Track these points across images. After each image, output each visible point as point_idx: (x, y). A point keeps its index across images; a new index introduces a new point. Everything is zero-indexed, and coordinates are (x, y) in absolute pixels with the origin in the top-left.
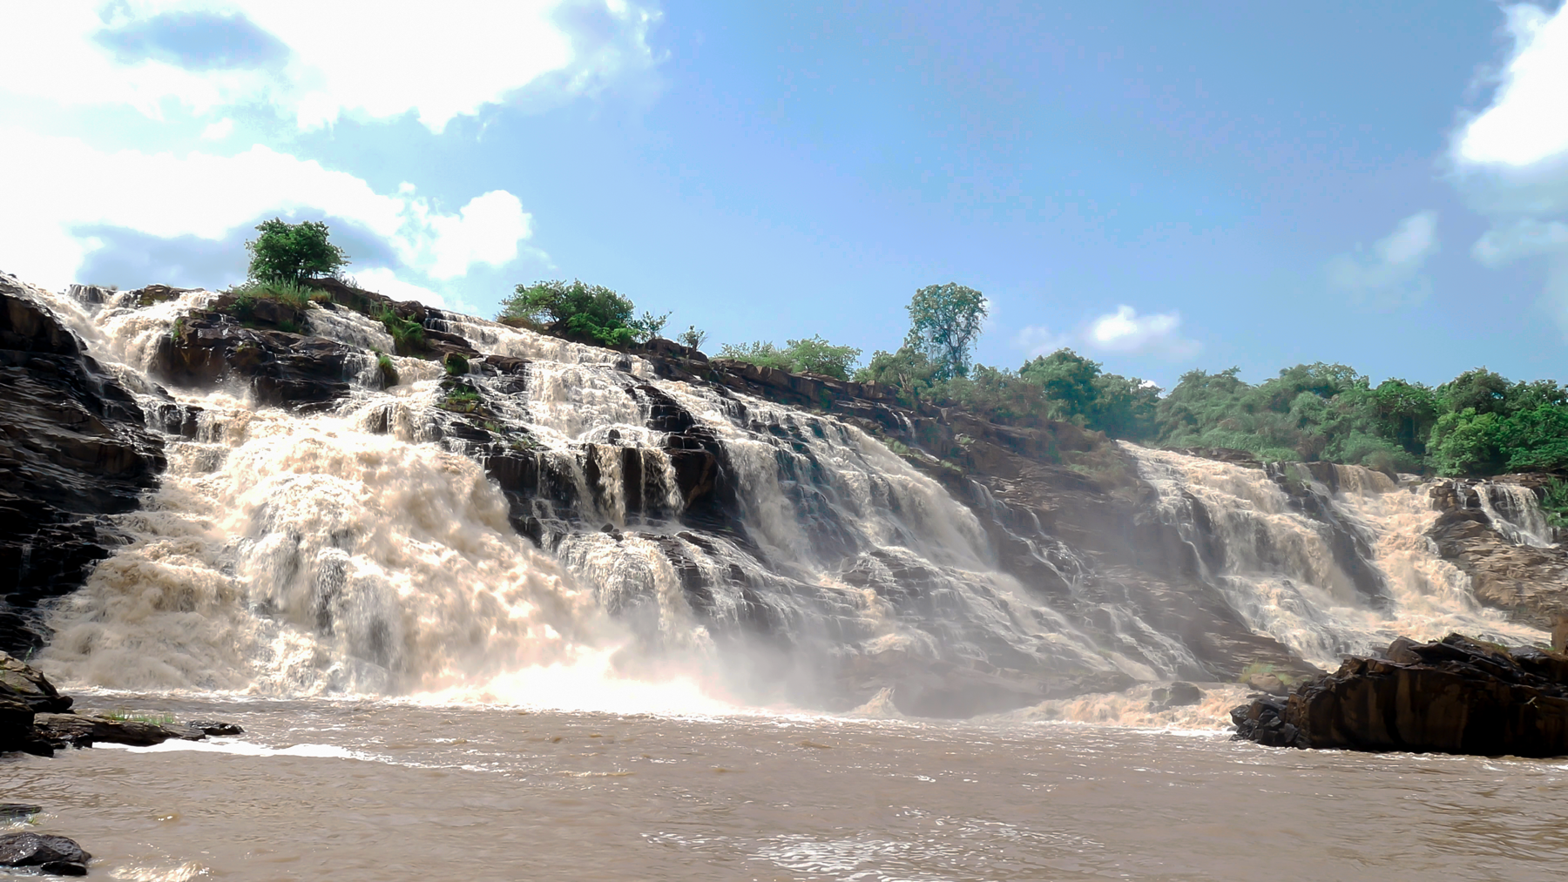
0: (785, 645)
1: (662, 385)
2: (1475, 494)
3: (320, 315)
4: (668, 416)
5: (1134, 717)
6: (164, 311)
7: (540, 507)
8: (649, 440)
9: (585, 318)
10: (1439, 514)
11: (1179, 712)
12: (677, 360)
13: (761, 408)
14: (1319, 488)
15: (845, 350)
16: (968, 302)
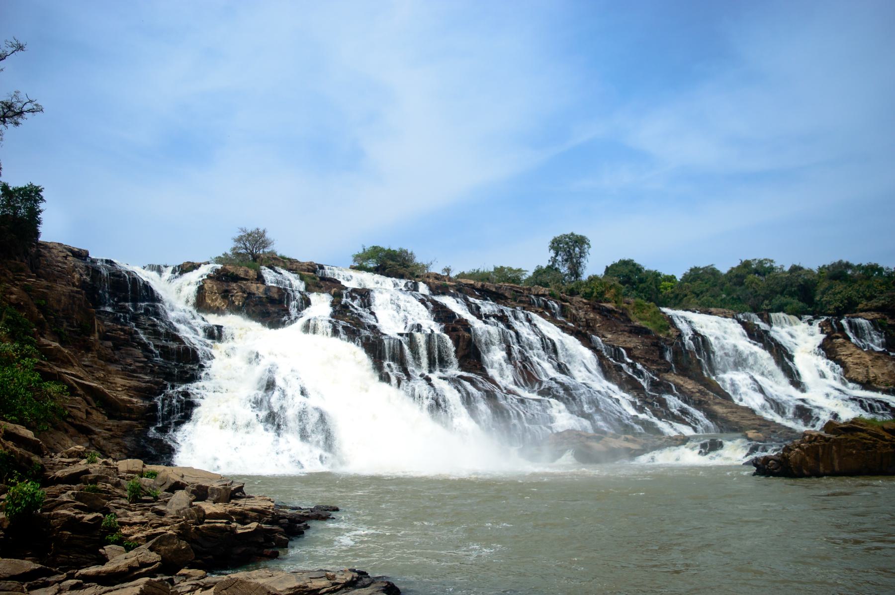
0: (509, 429)
1: (436, 298)
2: (842, 325)
3: (269, 275)
4: (442, 314)
5: (690, 457)
6: (194, 277)
7: (389, 366)
8: (430, 324)
9: (391, 263)
10: (824, 336)
11: (712, 454)
12: (440, 286)
13: (488, 307)
14: (764, 326)
15: (520, 270)
16: (580, 241)
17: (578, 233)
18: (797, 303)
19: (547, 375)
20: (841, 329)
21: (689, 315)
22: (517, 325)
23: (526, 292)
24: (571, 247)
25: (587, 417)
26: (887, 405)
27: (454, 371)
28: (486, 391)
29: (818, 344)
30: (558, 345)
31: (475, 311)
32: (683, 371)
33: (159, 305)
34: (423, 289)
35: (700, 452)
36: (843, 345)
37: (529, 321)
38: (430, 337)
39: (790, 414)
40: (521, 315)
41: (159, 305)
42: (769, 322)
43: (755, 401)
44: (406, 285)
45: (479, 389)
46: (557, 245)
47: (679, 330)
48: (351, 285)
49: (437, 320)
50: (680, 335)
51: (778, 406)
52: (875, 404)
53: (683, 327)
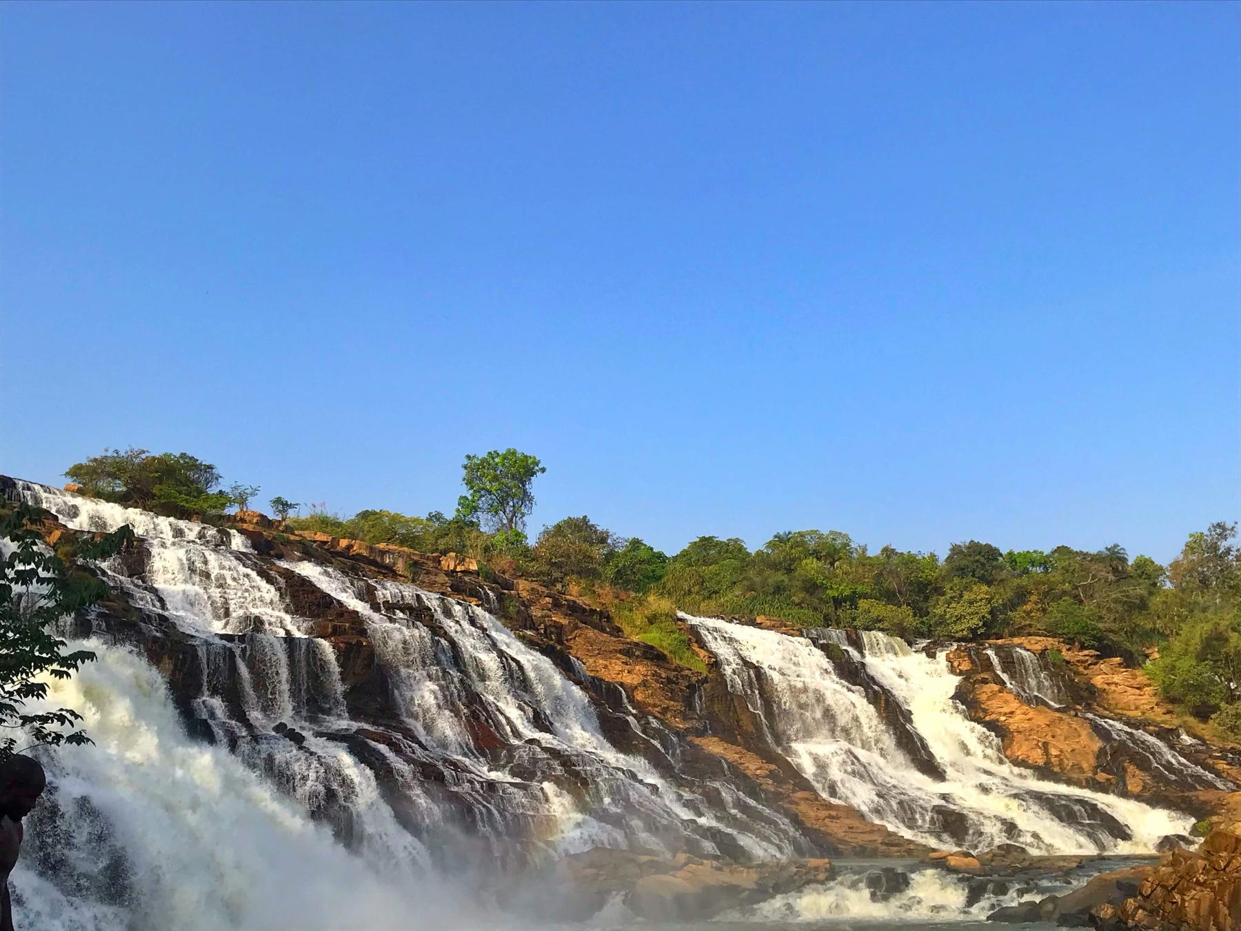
4: (301, 597)
8: (283, 623)
17: (523, 449)
18: (905, 614)
20: (988, 666)
21: (735, 630)
22: (449, 625)
23: (431, 564)
24: (506, 479)
25: (617, 821)
26: (1094, 807)
28: (423, 765)
29: (952, 692)
30: (532, 675)
31: (367, 595)
32: (728, 734)
34: (238, 542)
35: (873, 895)
36: (993, 695)
39: (924, 820)
40: (457, 609)
42: (859, 647)
43: (861, 796)
44: (201, 536)
45: (409, 761)
46: (476, 471)
47: (713, 655)
49: (296, 609)
50: (716, 664)
51: (907, 811)
52: (1077, 808)
53: (722, 650)
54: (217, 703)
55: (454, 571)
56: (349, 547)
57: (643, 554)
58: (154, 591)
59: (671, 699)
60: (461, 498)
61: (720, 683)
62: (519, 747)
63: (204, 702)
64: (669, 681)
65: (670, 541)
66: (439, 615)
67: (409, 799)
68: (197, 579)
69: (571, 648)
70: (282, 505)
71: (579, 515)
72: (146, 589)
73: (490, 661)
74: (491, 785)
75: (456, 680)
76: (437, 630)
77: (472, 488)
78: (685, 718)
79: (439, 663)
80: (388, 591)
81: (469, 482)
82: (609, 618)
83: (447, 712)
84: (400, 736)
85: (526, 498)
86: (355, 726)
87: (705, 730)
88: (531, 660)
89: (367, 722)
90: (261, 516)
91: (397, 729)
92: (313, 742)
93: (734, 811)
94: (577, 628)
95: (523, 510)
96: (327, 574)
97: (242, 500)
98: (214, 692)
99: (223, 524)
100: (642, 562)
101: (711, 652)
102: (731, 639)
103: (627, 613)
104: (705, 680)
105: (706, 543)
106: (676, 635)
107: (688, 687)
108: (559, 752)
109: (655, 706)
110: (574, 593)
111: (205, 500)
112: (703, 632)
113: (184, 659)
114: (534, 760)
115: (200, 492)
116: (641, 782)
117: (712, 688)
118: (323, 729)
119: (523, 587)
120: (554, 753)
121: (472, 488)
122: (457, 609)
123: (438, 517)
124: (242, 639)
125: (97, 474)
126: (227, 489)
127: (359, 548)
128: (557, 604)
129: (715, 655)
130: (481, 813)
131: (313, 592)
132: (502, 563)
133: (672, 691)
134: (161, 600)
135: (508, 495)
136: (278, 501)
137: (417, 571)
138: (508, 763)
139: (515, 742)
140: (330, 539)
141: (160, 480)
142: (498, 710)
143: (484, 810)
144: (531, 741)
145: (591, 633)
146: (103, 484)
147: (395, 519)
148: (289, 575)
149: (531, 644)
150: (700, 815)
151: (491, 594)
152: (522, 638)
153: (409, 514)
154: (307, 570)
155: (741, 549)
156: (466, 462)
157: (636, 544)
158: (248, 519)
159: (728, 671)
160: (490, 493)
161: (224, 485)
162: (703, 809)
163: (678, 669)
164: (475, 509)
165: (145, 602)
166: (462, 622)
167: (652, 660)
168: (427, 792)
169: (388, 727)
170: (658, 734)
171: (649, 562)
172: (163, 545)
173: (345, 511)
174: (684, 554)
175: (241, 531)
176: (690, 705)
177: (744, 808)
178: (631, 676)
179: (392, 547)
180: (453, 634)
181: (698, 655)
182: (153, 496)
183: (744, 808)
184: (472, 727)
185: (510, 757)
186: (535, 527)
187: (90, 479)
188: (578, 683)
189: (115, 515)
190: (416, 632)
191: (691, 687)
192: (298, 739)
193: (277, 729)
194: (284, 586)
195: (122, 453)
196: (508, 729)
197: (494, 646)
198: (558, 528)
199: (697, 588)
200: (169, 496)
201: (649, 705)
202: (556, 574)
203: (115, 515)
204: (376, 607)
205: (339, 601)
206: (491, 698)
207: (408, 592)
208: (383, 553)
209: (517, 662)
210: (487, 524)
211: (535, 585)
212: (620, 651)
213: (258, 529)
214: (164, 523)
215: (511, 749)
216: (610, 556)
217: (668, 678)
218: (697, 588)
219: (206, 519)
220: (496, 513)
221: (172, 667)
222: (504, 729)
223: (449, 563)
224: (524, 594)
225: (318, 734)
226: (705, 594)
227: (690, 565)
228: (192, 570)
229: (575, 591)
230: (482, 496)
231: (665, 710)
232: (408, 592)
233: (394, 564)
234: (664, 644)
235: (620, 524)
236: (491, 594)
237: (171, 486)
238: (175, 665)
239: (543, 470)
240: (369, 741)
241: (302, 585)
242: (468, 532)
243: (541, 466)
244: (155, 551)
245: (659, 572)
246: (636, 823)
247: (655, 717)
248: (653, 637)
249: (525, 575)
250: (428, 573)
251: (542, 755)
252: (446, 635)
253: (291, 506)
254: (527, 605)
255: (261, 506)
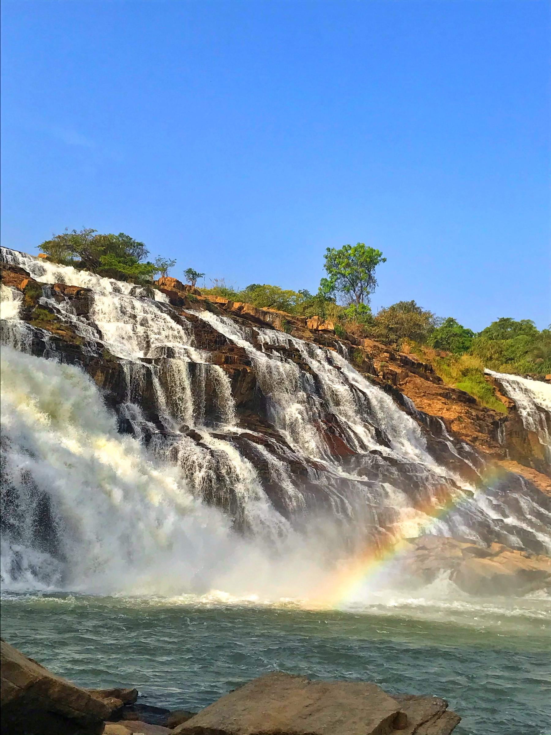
4: (204, 337)
8: (187, 353)
17: (369, 244)
19: (363, 446)
22: (314, 365)
23: (300, 324)
24: (357, 267)
27: (231, 427)
31: (253, 338)
33: (391, 535)
37: (330, 361)
38: (192, 367)
40: (319, 352)
41: (391, 535)
44: (132, 293)
45: (281, 458)
46: (334, 261)
48: (48, 278)
49: (199, 345)
50: (514, 408)
53: (518, 396)
54: (136, 408)
55: (317, 330)
56: (241, 308)
57: (455, 330)
58: (96, 327)
59: (479, 431)
60: (323, 279)
61: (518, 422)
62: (364, 456)
63: (127, 407)
64: (478, 418)
65: (477, 322)
66: (305, 355)
67: (281, 489)
68: (126, 318)
69: (403, 390)
70: (193, 275)
71: (407, 299)
72: (89, 324)
73: (342, 390)
74: (344, 481)
75: (317, 403)
76: (303, 366)
77: (331, 272)
78: (490, 447)
79: (305, 390)
80: (266, 336)
81: (329, 269)
82: (432, 371)
83: (309, 426)
84: (274, 440)
85: (370, 280)
86: (240, 431)
87: (505, 456)
88: (375, 393)
89: (250, 429)
90: (177, 281)
91: (271, 435)
92: (207, 438)
93: (529, 517)
94: (407, 376)
95: (368, 289)
96: (222, 322)
97: (164, 270)
98: (134, 400)
99: (147, 287)
100: (455, 335)
101: (511, 399)
102: (526, 390)
103: (445, 367)
104: (506, 420)
105: (504, 323)
106: (484, 385)
107: (492, 424)
108: (396, 461)
109: (467, 436)
110: (406, 351)
111: (136, 268)
112: (504, 384)
113: (113, 372)
114: (376, 466)
115: (133, 262)
116: (459, 488)
117: (512, 425)
118: (217, 432)
119: (368, 344)
120: (392, 462)
121: (331, 272)
122: (319, 352)
123: (305, 294)
124: (157, 361)
125: (60, 247)
126: (153, 261)
127: (248, 309)
128: (392, 358)
129: (514, 402)
130: (336, 502)
131: (212, 332)
132: (353, 327)
133: (480, 426)
134: (99, 332)
135: (357, 278)
136: (190, 271)
137: (289, 326)
138: (356, 467)
139: (363, 452)
140: (227, 302)
141: (105, 253)
142: (350, 428)
143: (338, 499)
144: (375, 452)
145: (419, 380)
146: (67, 255)
147: (274, 291)
148: (194, 319)
149: (374, 382)
150: (506, 516)
151: (344, 347)
152: (368, 378)
153: (284, 288)
154: (207, 316)
155: (531, 328)
156: (326, 253)
157: (451, 322)
158: (168, 283)
159: (524, 413)
160: (344, 276)
161: (151, 258)
162: (507, 512)
163: (485, 410)
164: (333, 288)
165: (86, 333)
166: (322, 362)
167: (465, 402)
168: (294, 483)
169: (265, 433)
170: (468, 455)
171: (460, 336)
172: (103, 294)
173: (239, 286)
174: (487, 331)
175: (163, 291)
176: (494, 437)
177: (539, 515)
178: (448, 413)
179: (271, 310)
180: (315, 370)
181: (500, 400)
182: (100, 263)
183: (539, 515)
184: (329, 439)
185: (358, 463)
186: (379, 302)
187: (55, 251)
188: (409, 413)
189: (78, 278)
190: (287, 365)
191: (496, 424)
192: (196, 437)
193: (181, 430)
194: (190, 327)
195: (78, 233)
196: (356, 443)
197: (346, 380)
198: (393, 309)
199: (497, 355)
200: (111, 264)
201: (463, 434)
202: (393, 337)
203: (78, 278)
204: (258, 347)
205: (231, 341)
206: (343, 419)
207: (283, 337)
208: (265, 313)
209: (364, 393)
210: (341, 299)
211: (376, 344)
212: (440, 395)
213: (174, 290)
214: (106, 283)
215: (359, 457)
216: (432, 330)
217: (477, 416)
218: (497, 355)
219: (135, 280)
220: (348, 291)
221: (103, 378)
222: (353, 442)
223: (313, 324)
224: (368, 349)
225: (216, 436)
226: (506, 360)
227: (491, 339)
228: (124, 313)
229: (406, 349)
230: (338, 279)
231: (475, 439)
232: (283, 337)
233: (273, 322)
234: (474, 391)
235: (439, 308)
236: (344, 347)
237: (112, 257)
238: (106, 378)
239: (384, 260)
240: (250, 442)
241: (204, 327)
242: (328, 305)
243: (382, 257)
244: (96, 297)
245: (467, 344)
246: (457, 518)
247: (467, 444)
248: (466, 386)
249: (368, 336)
250: (298, 329)
251: (382, 462)
252: (310, 370)
253: (199, 276)
254: (371, 357)
255: (177, 274)
